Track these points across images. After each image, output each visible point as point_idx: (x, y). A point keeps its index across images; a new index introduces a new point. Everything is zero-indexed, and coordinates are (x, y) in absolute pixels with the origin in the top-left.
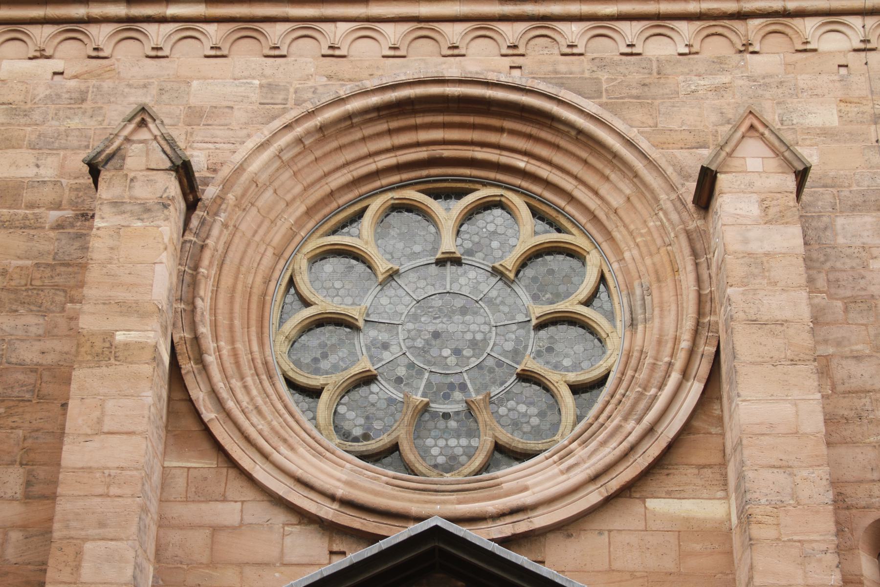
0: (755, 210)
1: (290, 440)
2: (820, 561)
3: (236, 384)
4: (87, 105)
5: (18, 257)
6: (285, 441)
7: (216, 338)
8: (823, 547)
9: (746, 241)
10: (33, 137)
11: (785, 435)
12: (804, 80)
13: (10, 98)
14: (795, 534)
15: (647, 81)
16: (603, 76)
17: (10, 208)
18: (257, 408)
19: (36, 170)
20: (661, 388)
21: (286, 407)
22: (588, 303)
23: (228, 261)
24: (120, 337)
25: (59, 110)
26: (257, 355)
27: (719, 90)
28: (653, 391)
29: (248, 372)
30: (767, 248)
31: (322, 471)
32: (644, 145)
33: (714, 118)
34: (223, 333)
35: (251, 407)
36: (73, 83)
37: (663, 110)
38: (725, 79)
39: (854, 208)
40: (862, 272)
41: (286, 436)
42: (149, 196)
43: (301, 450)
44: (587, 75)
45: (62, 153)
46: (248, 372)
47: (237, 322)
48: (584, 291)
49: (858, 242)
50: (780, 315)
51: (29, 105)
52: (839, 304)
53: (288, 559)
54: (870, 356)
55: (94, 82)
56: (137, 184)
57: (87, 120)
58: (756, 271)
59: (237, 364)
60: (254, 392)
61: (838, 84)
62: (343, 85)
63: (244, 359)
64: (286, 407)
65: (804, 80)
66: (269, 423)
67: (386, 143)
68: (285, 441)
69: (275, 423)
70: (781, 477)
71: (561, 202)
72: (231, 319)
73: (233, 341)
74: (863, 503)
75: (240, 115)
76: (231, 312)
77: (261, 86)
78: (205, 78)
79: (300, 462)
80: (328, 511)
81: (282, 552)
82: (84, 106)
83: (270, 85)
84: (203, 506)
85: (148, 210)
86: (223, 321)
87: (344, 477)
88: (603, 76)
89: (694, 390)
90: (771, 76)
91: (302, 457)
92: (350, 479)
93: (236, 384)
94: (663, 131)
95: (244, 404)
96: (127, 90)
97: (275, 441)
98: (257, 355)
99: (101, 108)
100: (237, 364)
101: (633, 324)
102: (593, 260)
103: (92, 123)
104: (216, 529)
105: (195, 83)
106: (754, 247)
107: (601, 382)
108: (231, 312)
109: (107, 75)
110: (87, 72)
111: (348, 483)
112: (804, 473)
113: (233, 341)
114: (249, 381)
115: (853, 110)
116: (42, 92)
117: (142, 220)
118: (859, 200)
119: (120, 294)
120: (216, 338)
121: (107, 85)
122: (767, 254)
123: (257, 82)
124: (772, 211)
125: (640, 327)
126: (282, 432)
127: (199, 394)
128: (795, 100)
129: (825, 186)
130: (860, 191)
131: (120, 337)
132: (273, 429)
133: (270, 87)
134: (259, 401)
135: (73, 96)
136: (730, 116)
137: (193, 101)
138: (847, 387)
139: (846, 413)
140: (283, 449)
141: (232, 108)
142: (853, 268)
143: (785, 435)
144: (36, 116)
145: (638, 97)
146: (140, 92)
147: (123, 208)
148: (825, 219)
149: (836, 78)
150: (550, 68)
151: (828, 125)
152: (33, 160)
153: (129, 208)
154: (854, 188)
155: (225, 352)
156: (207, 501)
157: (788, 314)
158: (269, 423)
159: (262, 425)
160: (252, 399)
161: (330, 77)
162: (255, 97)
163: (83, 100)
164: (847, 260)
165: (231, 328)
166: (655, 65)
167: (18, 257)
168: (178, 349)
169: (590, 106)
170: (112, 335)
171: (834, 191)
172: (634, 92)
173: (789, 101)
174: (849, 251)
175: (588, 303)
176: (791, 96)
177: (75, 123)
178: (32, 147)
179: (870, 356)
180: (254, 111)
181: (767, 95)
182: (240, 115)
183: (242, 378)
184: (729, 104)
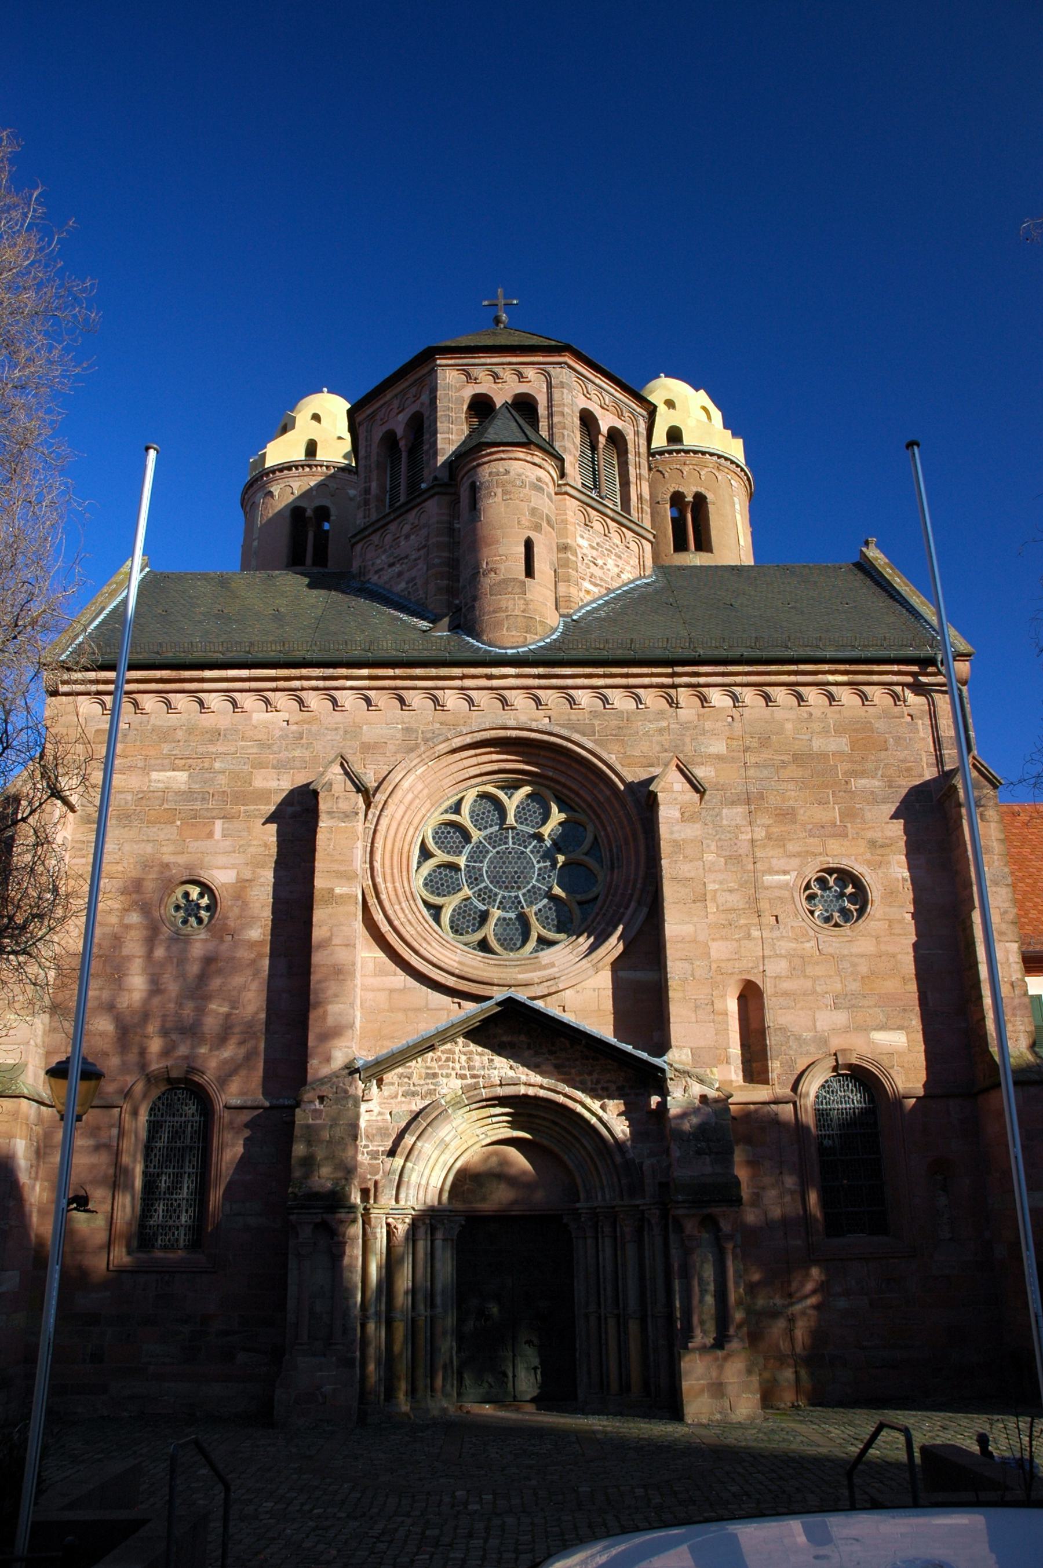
0: (678, 815)
1: (428, 939)
2: (704, 1009)
3: (397, 907)
4: (304, 741)
5: (857, 1540)
6: (425, 939)
7: (385, 882)
8: (706, 1002)
9: (672, 833)
10: (275, 762)
11: (689, 942)
12: (708, 725)
13: (260, 737)
14: (692, 995)
15: (621, 725)
16: (596, 722)
17: (265, 805)
18: (409, 920)
19: (278, 782)
20: (627, 908)
21: (423, 917)
22: (586, 854)
23: (388, 836)
24: (338, 891)
25: (287, 744)
26: (407, 889)
27: (660, 731)
28: (622, 910)
29: (402, 899)
30: (683, 836)
31: (446, 956)
32: (618, 768)
33: (658, 748)
34: (389, 878)
35: (405, 920)
36: (294, 728)
37: (630, 744)
38: (664, 724)
39: (733, 803)
40: (736, 841)
41: (425, 936)
42: (347, 807)
43: (434, 944)
44: (587, 722)
45: (292, 771)
46: (402, 899)
47: (395, 871)
48: (586, 846)
49: (733, 823)
50: (689, 875)
51: (270, 742)
52: (722, 859)
53: (430, 1006)
54: (738, 890)
55: (306, 726)
56: (340, 800)
57: (304, 751)
58: (677, 850)
59: (397, 895)
60: (407, 912)
61: (726, 728)
62: (450, 729)
63: (400, 891)
64: (423, 917)
65: (708, 725)
66: (416, 929)
67: (474, 761)
68: (425, 939)
69: (419, 929)
70: (686, 965)
71: (573, 796)
72: (392, 869)
73: (394, 883)
74: (730, 972)
75: (391, 747)
76: (392, 865)
77: (402, 729)
78: (370, 724)
79: (434, 952)
80: (451, 981)
81: (427, 1003)
82: (302, 741)
83: (407, 728)
84: (384, 978)
85: (347, 816)
86: (388, 871)
87: (457, 959)
88: (596, 722)
89: (645, 910)
90: (690, 723)
91: (434, 948)
92: (461, 960)
93: (397, 907)
94: (629, 757)
95: (402, 920)
96: (326, 732)
97: (420, 940)
98: (407, 889)
99: (311, 743)
100: (397, 895)
101: (612, 868)
102: (590, 828)
103: (307, 753)
104: (391, 991)
105: (365, 727)
106: (676, 836)
107: (596, 898)
108: (392, 865)
109: (314, 722)
110: (302, 721)
111: (459, 963)
112: (698, 963)
113: (394, 883)
114: (404, 905)
115: (735, 743)
116: (278, 733)
117: (344, 822)
118: (735, 799)
119: (336, 867)
120: (385, 882)
121: (314, 728)
122: (683, 840)
123: (400, 726)
124: (686, 815)
125: (616, 871)
126: (423, 934)
127: (379, 917)
128: (703, 737)
129: (718, 790)
130: (737, 793)
131: (338, 891)
132: (418, 932)
133: (407, 730)
134: (410, 916)
135: (296, 735)
136: (667, 747)
137: (365, 739)
138: (724, 908)
139: (723, 922)
140: (425, 945)
141: (386, 743)
142: (730, 839)
143: (689, 942)
144: (275, 748)
145: (616, 736)
146: (334, 733)
147: (333, 815)
148: (716, 810)
149: (725, 724)
150: (567, 718)
151: (720, 753)
152: (275, 776)
153: (337, 815)
154: (733, 791)
155: (390, 889)
156: (386, 976)
157: (692, 875)
158: (416, 929)
159: (413, 932)
160: (406, 916)
161: (441, 724)
162: (399, 736)
163: (302, 738)
164: (728, 834)
165: (392, 874)
166: (625, 715)
167: (857, 1540)
168: (366, 891)
169: (590, 745)
170: (332, 890)
171: (722, 792)
172: (614, 732)
173: (699, 737)
174: (729, 829)
175: (586, 854)
176: (701, 735)
177: (297, 753)
178: (274, 768)
179: (738, 890)
180: (399, 745)
181: (688, 734)
182: (391, 747)
183: (400, 904)
184: (666, 740)
